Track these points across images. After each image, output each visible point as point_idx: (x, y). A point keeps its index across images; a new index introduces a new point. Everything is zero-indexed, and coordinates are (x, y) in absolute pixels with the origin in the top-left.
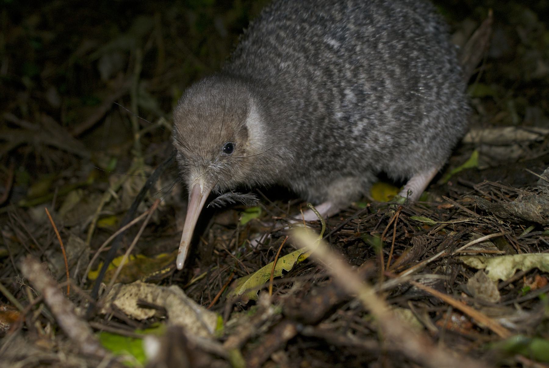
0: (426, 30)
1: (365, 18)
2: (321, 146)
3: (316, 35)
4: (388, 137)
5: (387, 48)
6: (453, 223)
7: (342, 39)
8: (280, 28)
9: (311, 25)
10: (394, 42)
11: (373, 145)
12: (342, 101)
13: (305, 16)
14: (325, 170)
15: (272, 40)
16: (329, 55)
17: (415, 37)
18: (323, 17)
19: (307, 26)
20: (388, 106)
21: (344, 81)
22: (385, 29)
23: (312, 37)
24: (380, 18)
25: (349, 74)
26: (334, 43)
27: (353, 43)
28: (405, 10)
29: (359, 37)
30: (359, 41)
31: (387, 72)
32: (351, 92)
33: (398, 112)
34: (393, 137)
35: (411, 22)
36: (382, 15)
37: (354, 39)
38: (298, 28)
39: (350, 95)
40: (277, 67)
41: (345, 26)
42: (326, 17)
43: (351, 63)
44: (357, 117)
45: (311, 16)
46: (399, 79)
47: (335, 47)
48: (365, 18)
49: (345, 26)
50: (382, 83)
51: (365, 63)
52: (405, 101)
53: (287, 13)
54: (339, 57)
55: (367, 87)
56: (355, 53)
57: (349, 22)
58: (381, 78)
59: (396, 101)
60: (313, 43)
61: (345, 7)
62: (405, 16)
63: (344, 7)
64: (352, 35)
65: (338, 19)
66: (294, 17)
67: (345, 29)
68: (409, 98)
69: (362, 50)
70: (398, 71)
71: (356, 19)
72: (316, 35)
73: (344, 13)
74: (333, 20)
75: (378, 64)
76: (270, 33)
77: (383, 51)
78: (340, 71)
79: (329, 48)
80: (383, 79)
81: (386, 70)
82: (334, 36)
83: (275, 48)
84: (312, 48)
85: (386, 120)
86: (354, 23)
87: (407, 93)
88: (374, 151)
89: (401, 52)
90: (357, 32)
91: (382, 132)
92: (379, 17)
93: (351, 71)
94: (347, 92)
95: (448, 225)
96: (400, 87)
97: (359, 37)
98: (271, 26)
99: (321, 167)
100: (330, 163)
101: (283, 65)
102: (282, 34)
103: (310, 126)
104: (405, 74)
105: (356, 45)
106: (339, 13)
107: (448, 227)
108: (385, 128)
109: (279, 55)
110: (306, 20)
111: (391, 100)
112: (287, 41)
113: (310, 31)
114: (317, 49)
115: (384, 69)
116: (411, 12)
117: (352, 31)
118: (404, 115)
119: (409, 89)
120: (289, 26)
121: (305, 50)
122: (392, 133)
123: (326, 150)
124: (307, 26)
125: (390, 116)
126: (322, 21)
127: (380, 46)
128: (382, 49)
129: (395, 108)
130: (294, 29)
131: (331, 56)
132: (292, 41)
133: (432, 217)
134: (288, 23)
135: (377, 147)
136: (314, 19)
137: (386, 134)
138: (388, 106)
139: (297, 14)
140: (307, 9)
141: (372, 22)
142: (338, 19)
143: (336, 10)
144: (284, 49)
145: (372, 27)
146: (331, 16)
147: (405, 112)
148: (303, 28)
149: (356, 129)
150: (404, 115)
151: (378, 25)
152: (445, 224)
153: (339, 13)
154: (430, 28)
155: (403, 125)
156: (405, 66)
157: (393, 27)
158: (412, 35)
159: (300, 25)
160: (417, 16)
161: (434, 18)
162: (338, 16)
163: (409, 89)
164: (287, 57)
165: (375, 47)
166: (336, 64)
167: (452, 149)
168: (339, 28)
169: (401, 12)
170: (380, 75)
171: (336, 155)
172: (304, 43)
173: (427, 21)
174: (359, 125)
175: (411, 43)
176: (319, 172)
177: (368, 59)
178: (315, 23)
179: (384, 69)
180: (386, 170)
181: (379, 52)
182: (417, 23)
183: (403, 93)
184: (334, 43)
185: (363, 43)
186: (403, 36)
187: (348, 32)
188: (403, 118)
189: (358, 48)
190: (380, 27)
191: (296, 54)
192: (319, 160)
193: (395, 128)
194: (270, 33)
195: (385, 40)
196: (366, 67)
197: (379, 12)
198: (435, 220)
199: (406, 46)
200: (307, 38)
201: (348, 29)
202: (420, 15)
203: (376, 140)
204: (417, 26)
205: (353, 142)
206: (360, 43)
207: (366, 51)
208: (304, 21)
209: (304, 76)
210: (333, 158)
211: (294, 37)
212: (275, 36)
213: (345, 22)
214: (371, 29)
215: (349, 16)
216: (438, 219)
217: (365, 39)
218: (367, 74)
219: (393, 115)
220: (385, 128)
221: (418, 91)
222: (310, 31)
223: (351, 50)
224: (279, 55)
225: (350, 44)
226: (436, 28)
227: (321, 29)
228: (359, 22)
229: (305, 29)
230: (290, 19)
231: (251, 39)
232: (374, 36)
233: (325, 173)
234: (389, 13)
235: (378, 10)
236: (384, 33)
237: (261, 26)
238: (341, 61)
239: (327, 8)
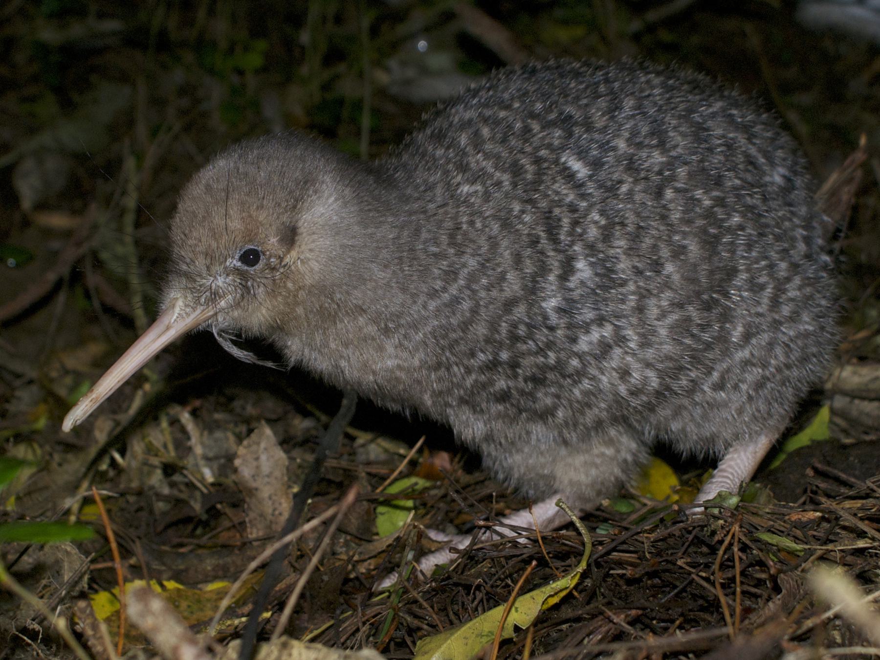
0: (767, 179)
1: (652, 134)
2: (504, 356)
3: (549, 146)
4: (651, 374)
5: (682, 202)
6: (836, 549)
7: (596, 165)
8: (486, 120)
9: (547, 125)
10: (699, 193)
11: (617, 382)
12: (564, 277)
13: (539, 106)
14: (512, 405)
15: (463, 139)
16: (561, 187)
17: (743, 188)
18: (570, 117)
19: (536, 126)
20: (663, 315)
21: (580, 243)
22: (686, 163)
23: (537, 149)
24: (680, 142)
25: (593, 233)
26: (578, 167)
27: (615, 176)
28: (731, 135)
29: (632, 166)
30: (630, 176)
31: (672, 247)
32: (587, 268)
33: (683, 327)
34: (661, 374)
35: (741, 158)
36: (684, 135)
37: (621, 168)
38: (518, 125)
39: (583, 269)
40: (451, 189)
41: (608, 142)
42: (577, 115)
43: (602, 213)
44: (589, 315)
45: (549, 110)
46: (695, 265)
47: (580, 175)
48: (652, 134)
49: (608, 142)
50: (657, 266)
51: (631, 218)
52: (698, 310)
53: (506, 96)
54: (583, 196)
55: (624, 265)
56: (616, 196)
57: (618, 136)
58: (654, 255)
59: (681, 306)
60: (538, 161)
61: (618, 108)
62: (730, 146)
63: (614, 108)
64: (618, 161)
65: (599, 125)
66: (516, 105)
67: (606, 147)
68: (708, 307)
69: (630, 193)
70: (694, 248)
71: (634, 133)
72: (549, 146)
73: (612, 118)
74: (589, 126)
75: (656, 227)
76: (466, 125)
77: (671, 206)
78: (575, 223)
79: (569, 176)
80: (660, 257)
81: (669, 242)
82: (581, 154)
83: (465, 154)
84: (530, 168)
85: (654, 339)
86: (628, 140)
87: (705, 297)
88: (616, 394)
89: (709, 214)
90: (631, 159)
91: (639, 361)
92: (679, 138)
93: (600, 227)
94: (580, 264)
95: (825, 554)
96: (694, 281)
97: (632, 166)
98: (468, 115)
99: (504, 397)
100: (522, 393)
101: (466, 189)
102: (486, 132)
103: (475, 311)
104: (709, 259)
105: (620, 182)
106: (603, 115)
107: (825, 556)
108: (650, 354)
109: (463, 168)
110: (539, 115)
111: (672, 304)
112: (488, 147)
113: (540, 135)
114: (540, 173)
115: (666, 241)
116: (741, 139)
117: (620, 152)
118: (693, 336)
119: (711, 289)
120: (503, 119)
121: (516, 170)
122: (660, 366)
123: (514, 365)
124: (536, 126)
125: (663, 332)
126: (566, 122)
127: (669, 194)
128: (671, 201)
129: (676, 320)
130: (510, 127)
131: (565, 192)
132: (499, 149)
133: (789, 535)
134: (502, 114)
135: (623, 390)
136: (552, 116)
137: (648, 365)
138: (663, 315)
139: (523, 102)
140: (545, 96)
141: (662, 145)
142: (599, 125)
143: (598, 109)
144: (477, 160)
145: (662, 153)
146: (587, 118)
147: (695, 331)
148: (527, 130)
149: (585, 339)
150: (693, 336)
151: (673, 153)
152: (822, 551)
153: (603, 115)
154: (777, 177)
155: (687, 355)
156: (710, 244)
157: (702, 161)
158: (738, 182)
159: (523, 121)
160: (753, 151)
161: (784, 160)
162: (600, 121)
163: (711, 289)
164: (479, 177)
165: (659, 194)
166: (573, 208)
167: (308, 372)
168: (597, 142)
169: (723, 136)
170: (655, 247)
171: (538, 380)
172: (519, 156)
173: (772, 164)
174: (594, 333)
175: (731, 200)
176: (500, 407)
177: (638, 214)
178: (553, 124)
179: (666, 241)
180: (664, 436)
181: (664, 207)
182: (751, 162)
183: (698, 294)
184: (578, 167)
185: (636, 181)
186: (718, 182)
187: (611, 154)
188: (688, 341)
189: (624, 188)
190: (676, 158)
191: (498, 174)
192: (501, 384)
193: (669, 358)
194: (466, 125)
195: (679, 185)
196: (630, 228)
197: (682, 129)
198: (797, 541)
199: (720, 202)
200: (528, 149)
201: (615, 149)
202: (760, 150)
203: (625, 373)
204: (750, 168)
205: (575, 362)
206: (631, 180)
207: (638, 197)
208: (533, 116)
209: (495, 217)
210: (530, 385)
211: (504, 141)
212: (470, 131)
213: (609, 134)
214: (658, 158)
215: (622, 125)
216: (803, 541)
217: (643, 174)
218: (628, 240)
219: (671, 332)
220: (650, 354)
221: (726, 295)
222: (540, 135)
223: (611, 190)
224: (463, 168)
225: (610, 176)
226: (788, 179)
227: (560, 137)
228: (638, 140)
229: (530, 130)
230: (508, 107)
231: (428, 131)
232: (660, 173)
233: (512, 412)
234: (699, 133)
235: (679, 126)
236: (682, 172)
237: (453, 111)
238: (584, 204)
239: (585, 101)
